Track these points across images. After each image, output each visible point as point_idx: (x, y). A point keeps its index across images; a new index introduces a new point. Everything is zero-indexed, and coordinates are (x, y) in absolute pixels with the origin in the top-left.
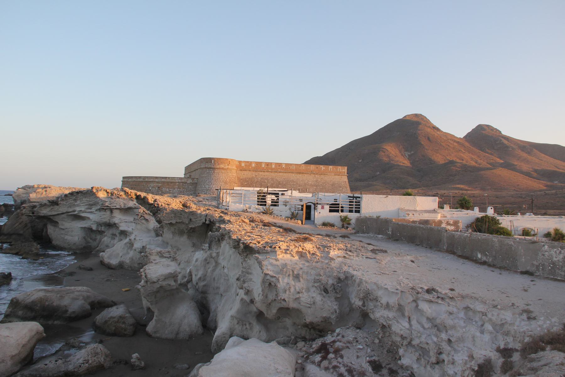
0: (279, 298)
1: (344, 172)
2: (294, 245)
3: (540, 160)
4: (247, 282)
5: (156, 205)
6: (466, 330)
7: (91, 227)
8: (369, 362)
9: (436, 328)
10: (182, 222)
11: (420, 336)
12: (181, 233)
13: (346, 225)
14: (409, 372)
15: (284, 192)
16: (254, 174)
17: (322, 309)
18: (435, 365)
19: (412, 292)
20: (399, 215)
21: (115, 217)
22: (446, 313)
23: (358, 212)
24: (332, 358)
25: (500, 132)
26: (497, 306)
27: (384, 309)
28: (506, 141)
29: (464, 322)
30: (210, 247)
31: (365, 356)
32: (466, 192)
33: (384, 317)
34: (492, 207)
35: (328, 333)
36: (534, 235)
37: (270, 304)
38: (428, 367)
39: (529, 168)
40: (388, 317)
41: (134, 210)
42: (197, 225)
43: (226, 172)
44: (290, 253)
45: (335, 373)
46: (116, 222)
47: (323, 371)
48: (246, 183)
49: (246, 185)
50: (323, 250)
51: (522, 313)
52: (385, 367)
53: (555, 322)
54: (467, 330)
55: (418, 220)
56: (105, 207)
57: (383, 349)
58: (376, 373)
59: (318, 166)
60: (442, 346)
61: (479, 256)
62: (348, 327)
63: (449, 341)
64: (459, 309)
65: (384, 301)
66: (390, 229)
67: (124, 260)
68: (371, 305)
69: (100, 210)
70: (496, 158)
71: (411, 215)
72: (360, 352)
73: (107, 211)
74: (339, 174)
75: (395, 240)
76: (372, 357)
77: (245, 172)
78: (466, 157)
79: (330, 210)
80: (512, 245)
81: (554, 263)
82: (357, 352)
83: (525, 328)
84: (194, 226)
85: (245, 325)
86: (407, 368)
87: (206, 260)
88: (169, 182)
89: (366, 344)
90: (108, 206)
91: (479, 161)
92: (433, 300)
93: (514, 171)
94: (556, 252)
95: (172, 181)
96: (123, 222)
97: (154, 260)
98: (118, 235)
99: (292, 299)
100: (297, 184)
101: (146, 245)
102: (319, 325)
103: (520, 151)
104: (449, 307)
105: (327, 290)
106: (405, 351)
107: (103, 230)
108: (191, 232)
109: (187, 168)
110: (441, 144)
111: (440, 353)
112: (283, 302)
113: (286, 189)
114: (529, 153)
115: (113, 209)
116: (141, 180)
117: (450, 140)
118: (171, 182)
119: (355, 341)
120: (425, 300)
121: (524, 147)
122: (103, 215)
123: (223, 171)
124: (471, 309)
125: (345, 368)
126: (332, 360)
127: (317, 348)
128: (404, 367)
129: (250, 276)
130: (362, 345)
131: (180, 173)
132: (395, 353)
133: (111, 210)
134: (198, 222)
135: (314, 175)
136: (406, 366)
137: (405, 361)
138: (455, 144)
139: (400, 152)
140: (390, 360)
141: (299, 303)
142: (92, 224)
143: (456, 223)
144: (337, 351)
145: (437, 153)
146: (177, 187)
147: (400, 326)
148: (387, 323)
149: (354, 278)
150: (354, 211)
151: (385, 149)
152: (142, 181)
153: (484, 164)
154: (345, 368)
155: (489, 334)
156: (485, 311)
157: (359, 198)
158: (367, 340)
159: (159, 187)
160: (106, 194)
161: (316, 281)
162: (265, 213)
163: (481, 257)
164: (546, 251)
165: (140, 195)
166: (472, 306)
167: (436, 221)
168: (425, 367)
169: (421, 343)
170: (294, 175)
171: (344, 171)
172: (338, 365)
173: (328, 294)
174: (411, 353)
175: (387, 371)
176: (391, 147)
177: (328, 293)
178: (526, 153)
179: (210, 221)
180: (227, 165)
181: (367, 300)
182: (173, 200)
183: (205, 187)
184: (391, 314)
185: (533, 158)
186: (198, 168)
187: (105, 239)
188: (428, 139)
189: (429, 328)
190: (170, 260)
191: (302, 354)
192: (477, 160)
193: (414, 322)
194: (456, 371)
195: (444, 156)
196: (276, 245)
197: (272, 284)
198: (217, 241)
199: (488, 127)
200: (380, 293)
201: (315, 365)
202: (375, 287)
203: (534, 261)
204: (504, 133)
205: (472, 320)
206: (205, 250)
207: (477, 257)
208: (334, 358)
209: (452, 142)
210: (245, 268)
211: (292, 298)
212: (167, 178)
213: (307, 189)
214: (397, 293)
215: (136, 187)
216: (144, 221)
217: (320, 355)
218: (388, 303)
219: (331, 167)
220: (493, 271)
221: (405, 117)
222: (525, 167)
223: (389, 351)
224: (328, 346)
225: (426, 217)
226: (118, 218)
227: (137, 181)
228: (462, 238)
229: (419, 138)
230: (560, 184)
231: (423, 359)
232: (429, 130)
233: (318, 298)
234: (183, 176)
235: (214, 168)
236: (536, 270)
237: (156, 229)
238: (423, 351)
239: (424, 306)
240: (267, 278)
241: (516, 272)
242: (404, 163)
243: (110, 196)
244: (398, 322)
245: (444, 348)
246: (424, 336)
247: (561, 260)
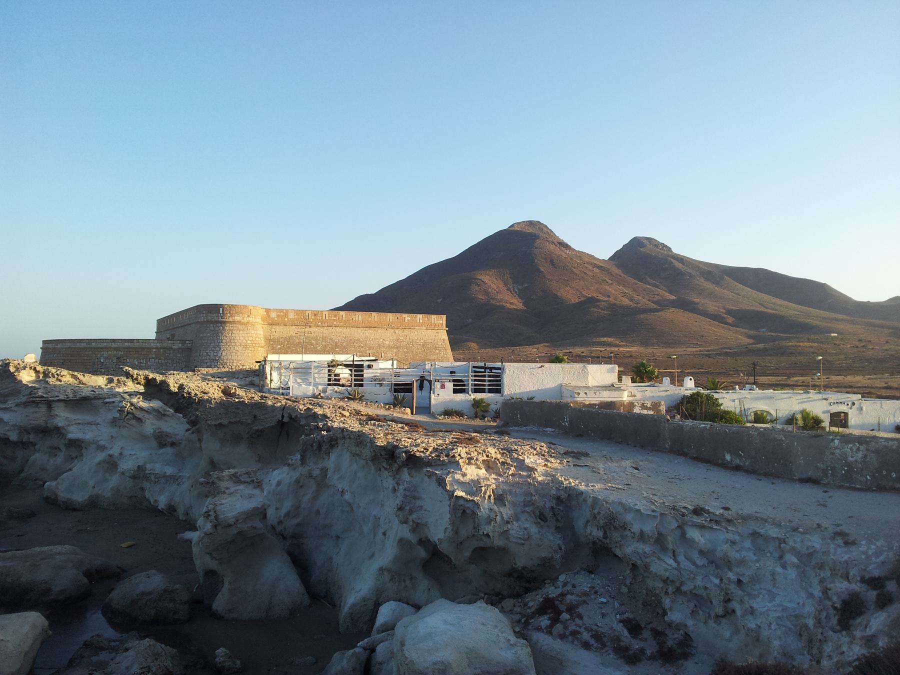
0: (481, 532)
1: (442, 324)
2: (476, 451)
3: (735, 293)
4: (416, 511)
5: (185, 395)
6: (760, 565)
7: (6, 436)
8: (621, 621)
9: (714, 565)
10: (239, 421)
11: (694, 578)
12: (236, 439)
13: (480, 414)
14: (681, 632)
15: (371, 363)
16: (292, 331)
17: (540, 546)
18: (721, 619)
19: (674, 514)
20: (562, 395)
21: (57, 415)
22: (727, 543)
23: (498, 391)
24: (566, 620)
25: (669, 249)
26: (798, 528)
27: (638, 541)
28: (680, 264)
29: (755, 554)
30: (303, 461)
31: (614, 614)
32: (617, 349)
33: (638, 553)
34: (691, 377)
35: (545, 583)
36: (772, 421)
37: (461, 543)
38: (711, 623)
39: (718, 307)
40: (645, 553)
41: (93, 401)
42: (267, 425)
43: (246, 329)
44: (476, 464)
45: (576, 642)
46: (60, 425)
47: (559, 640)
48: (279, 346)
49: (280, 349)
50: (510, 456)
51: (835, 537)
52: (645, 627)
53: (882, 546)
54: (762, 565)
55: (597, 402)
56: (37, 399)
57: (636, 602)
58: (635, 637)
59: (398, 315)
60: (730, 590)
61: (728, 457)
62: (576, 571)
63: (739, 582)
64: (742, 536)
65: (636, 528)
66: (567, 419)
67: (100, 492)
68: (616, 535)
69: (25, 404)
70: (664, 292)
71: (582, 395)
72: (604, 607)
73: (40, 405)
74: (433, 327)
75: (578, 436)
76: (623, 613)
77: (278, 328)
78: (613, 292)
79: (454, 389)
80: (783, 441)
81: (849, 465)
82: (601, 608)
83: (846, 557)
84: (262, 427)
85: (404, 581)
86: (678, 627)
87: (297, 481)
88: (139, 348)
89: (610, 596)
90: (42, 397)
91: (636, 298)
92: (706, 524)
93: (694, 313)
94: (851, 449)
95: (144, 345)
96: (72, 425)
97: (227, 488)
98: (64, 449)
99: (498, 533)
100: (366, 345)
101: (145, 464)
102: (533, 571)
103: (702, 280)
104: (728, 534)
105: (544, 516)
106: (672, 601)
107: (31, 440)
109: (161, 323)
110: (572, 271)
111: (728, 601)
112: (485, 539)
113: (373, 358)
114: (717, 283)
115: (53, 401)
116: (83, 345)
117: (587, 263)
118: (142, 348)
119: (593, 592)
120: (696, 526)
121: (709, 273)
122: (33, 413)
123: (240, 327)
124: (761, 536)
125: (588, 633)
126: (568, 623)
127: (537, 607)
128: (674, 625)
129: (419, 503)
130: (604, 598)
131: (149, 332)
132: (654, 605)
133: (49, 404)
134: (269, 420)
135: (392, 331)
136: (677, 623)
137: (675, 616)
138: (596, 270)
139: (505, 284)
140: (651, 617)
141: (508, 539)
142: (8, 430)
143: (655, 406)
144: (571, 609)
145: (566, 286)
146: (154, 356)
147: (664, 565)
148: (642, 562)
149: (581, 499)
150: (487, 391)
151: (480, 280)
152: (86, 348)
153: (644, 302)
154: (588, 633)
155: (795, 569)
156: (782, 537)
157: (500, 369)
158: (610, 589)
159: (118, 358)
160: (34, 375)
161: (526, 504)
162: (352, 399)
163: (731, 459)
164: (836, 448)
165: (155, 379)
166: (762, 531)
167: (625, 403)
168: (705, 623)
169: (695, 587)
170: (359, 330)
171: (441, 322)
172: (578, 629)
173: (546, 523)
174: (681, 604)
175: (650, 634)
176: (491, 277)
177: (547, 521)
178: (714, 283)
179: (290, 417)
180: (246, 316)
181: (610, 528)
182: (208, 384)
183: (208, 355)
184: (648, 549)
185: (725, 291)
186: (192, 322)
187: (37, 456)
188: (552, 262)
189: (704, 566)
190: (251, 486)
191: (517, 617)
192: (633, 297)
193: (681, 558)
194: (759, 625)
195: (577, 290)
196: (454, 451)
197: (468, 512)
198: (316, 450)
199: (649, 242)
200: (629, 517)
201: (543, 632)
202: (620, 509)
203: (818, 463)
204: (676, 250)
205: (764, 551)
206: (293, 465)
207: (724, 459)
208: (569, 619)
209: (591, 268)
210: (409, 490)
211: (498, 532)
213: (383, 354)
214: (655, 517)
215: (72, 358)
216: (133, 422)
217: (546, 617)
218: (641, 531)
219: (420, 316)
220: (761, 480)
221: (512, 226)
222: (712, 306)
223: (645, 604)
224: (557, 602)
225: (607, 396)
226: (62, 416)
227: (75, 348)
228: (697, 431)
229: (536, 261)
230: (769, 334)
231: (701, 612)
232: (552, 247)
233: (534, 530)
234: (153, 336)
235: (225, 322)
236: (822, 475)
237: (159, 434)
238: (699, 600)
239: (694, 534)
240: (460, 503)
241: (792, 480)
242: (511, 304)
243: (41, 378)
244: (659, 559)
245: (733, 593)
246: (699, 578)
247: (859, 460)
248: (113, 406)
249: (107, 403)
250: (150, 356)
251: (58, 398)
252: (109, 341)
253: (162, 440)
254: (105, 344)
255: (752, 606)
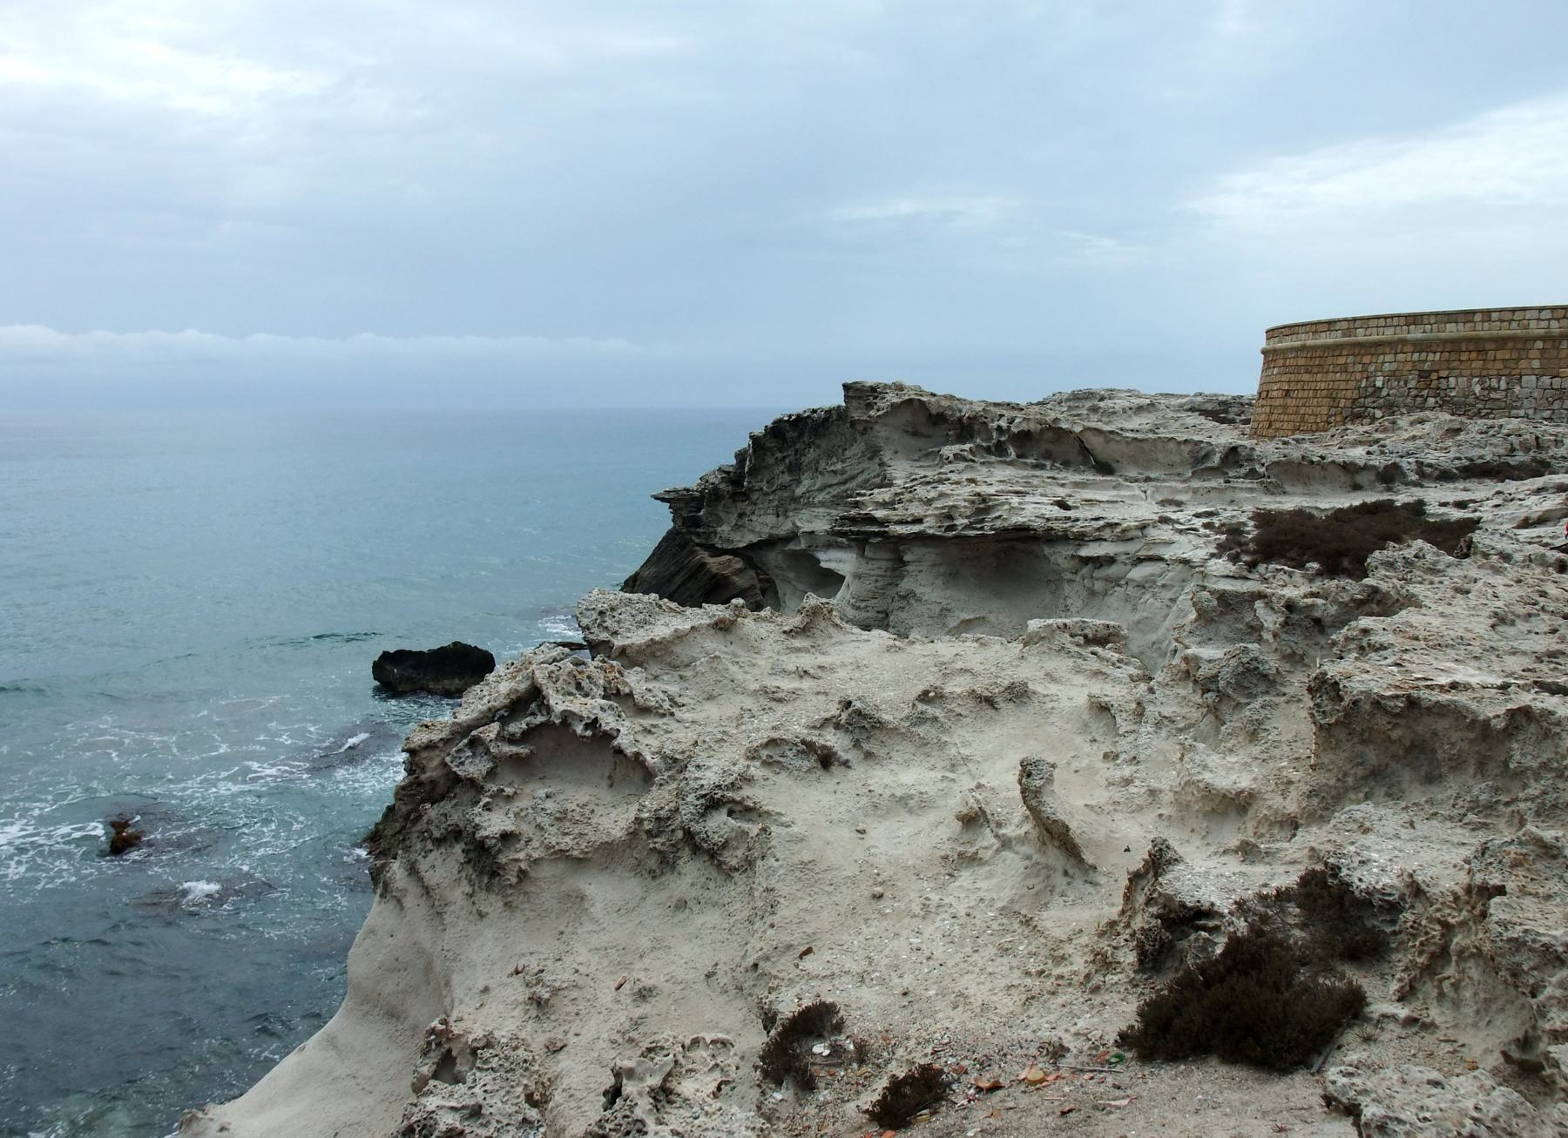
108: (1282, 824)
159: (1424, 375)
212: (1478, 317)
248: (1107, 579)
249: (1087, 561)
250: (1523, 364)
251: (916, 528)
252: (1402, 321)
253: (1368, 848)
254: (1390, 331)
255: (369, 879)
